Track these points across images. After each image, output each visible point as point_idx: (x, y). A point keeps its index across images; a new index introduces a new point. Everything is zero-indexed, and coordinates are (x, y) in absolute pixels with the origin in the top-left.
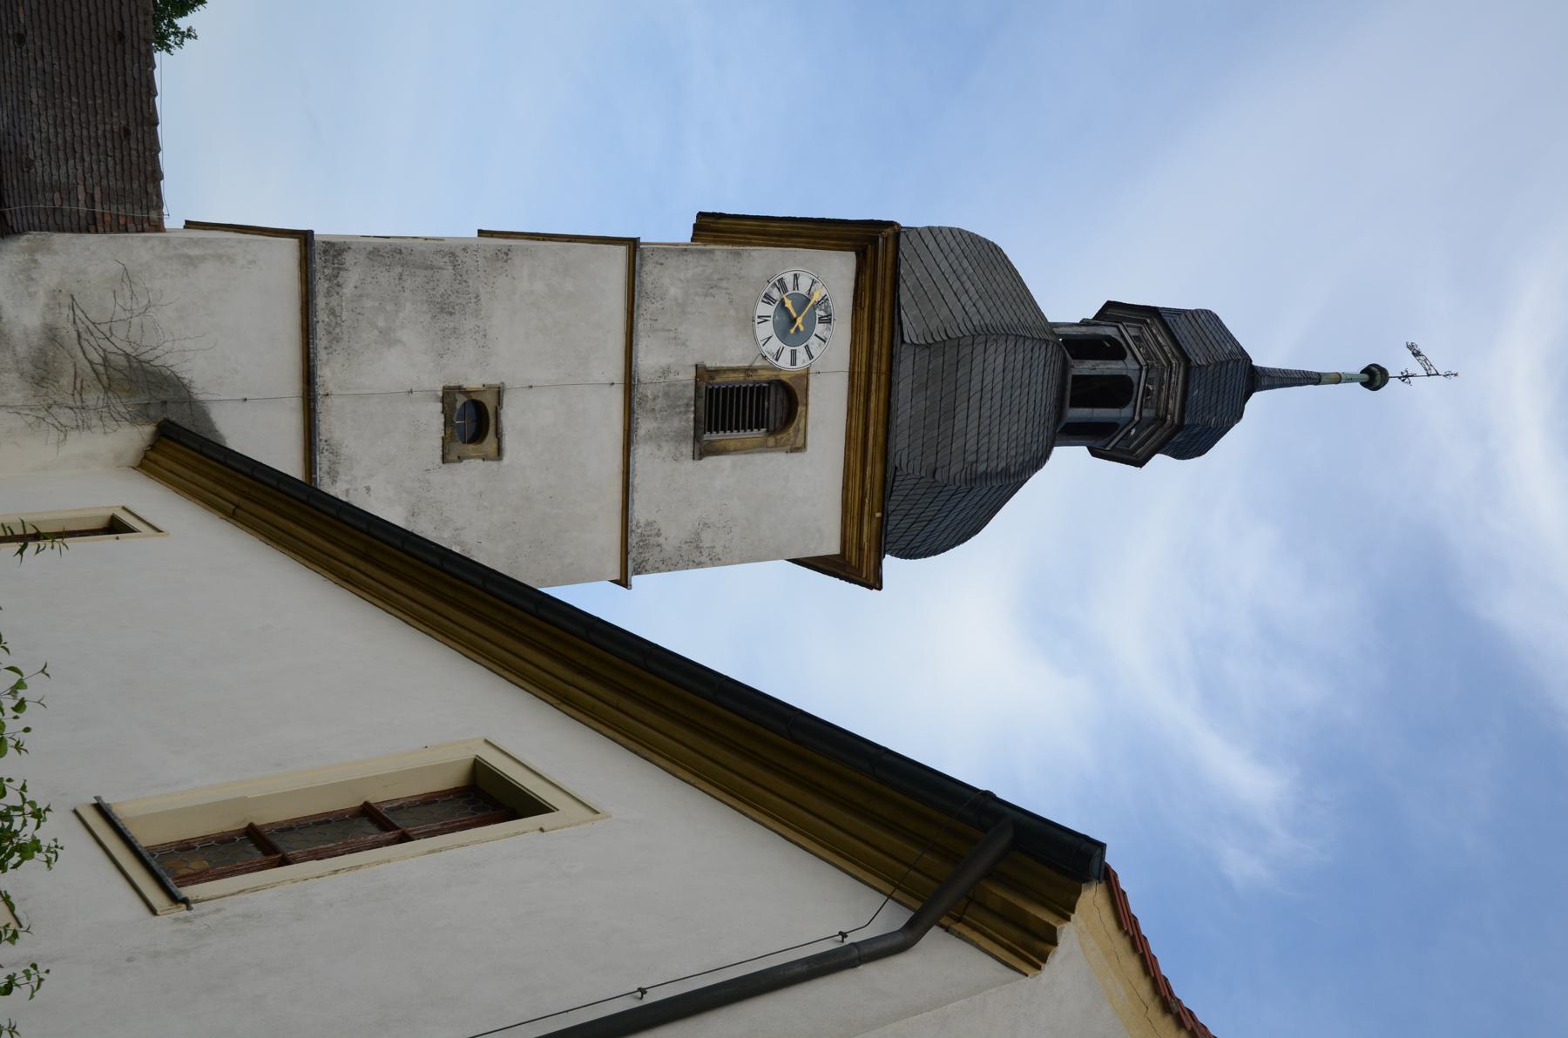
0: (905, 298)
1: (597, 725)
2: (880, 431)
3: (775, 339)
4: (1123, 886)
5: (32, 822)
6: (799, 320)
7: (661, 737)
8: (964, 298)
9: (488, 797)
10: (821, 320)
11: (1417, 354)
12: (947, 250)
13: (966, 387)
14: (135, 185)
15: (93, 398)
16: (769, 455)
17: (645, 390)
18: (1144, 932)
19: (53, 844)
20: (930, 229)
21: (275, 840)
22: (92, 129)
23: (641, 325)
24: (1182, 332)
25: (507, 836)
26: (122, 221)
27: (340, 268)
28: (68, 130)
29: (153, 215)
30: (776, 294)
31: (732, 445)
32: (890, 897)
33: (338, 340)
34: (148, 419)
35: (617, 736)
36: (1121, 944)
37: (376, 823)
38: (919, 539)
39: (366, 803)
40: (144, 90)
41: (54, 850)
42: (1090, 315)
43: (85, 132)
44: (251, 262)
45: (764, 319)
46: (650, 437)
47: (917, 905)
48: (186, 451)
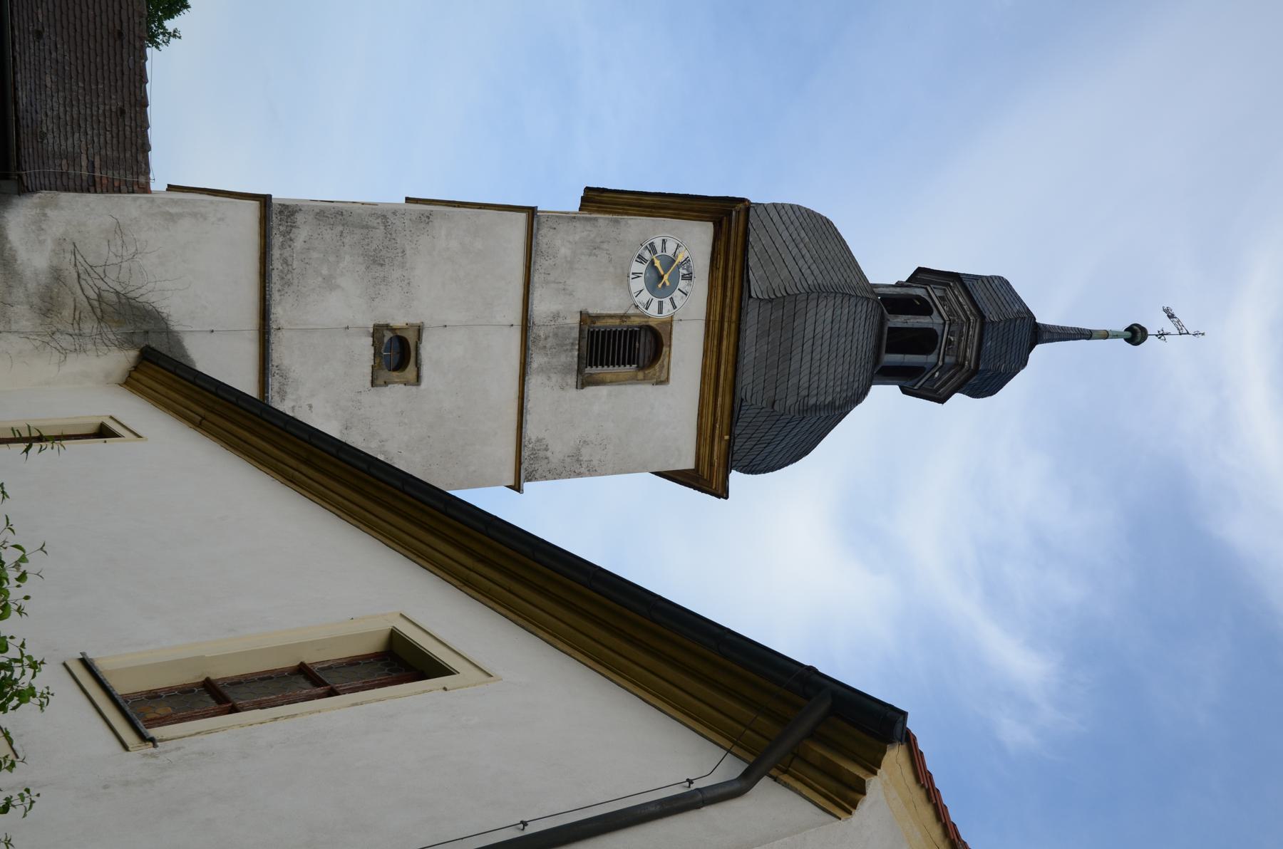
1: (420, 560)
2: (730, 369)
3: (645, 291)
4: (921, 747)
5: (29, 672)
6: (666, 277)
8: (801, 262)
9: (401, 661)
10: (684, 277)
11: (1171, 316)
13: (802, 337)
14: (128, 155)
15: (89, 326)
17: (538, 331)
20: (775, 205)
22: (95, 108)
23: (537, 278)
24: (979, 294)
26: (116, 184)
28: (75, 109)
29: (142, 179)
30: (647, 255)
31: (608, 377)
32: (729, 751)
33: (289, 284)
34: (133, 345)
36: (918, 795)
37: (310, 680)
39: (302, 664)
41: (46, 696)
42: (904, 279)
44: (220, 219)
45: (637, 275)
46: (542, 370)
47: (752, 759)
48: (164, 373)
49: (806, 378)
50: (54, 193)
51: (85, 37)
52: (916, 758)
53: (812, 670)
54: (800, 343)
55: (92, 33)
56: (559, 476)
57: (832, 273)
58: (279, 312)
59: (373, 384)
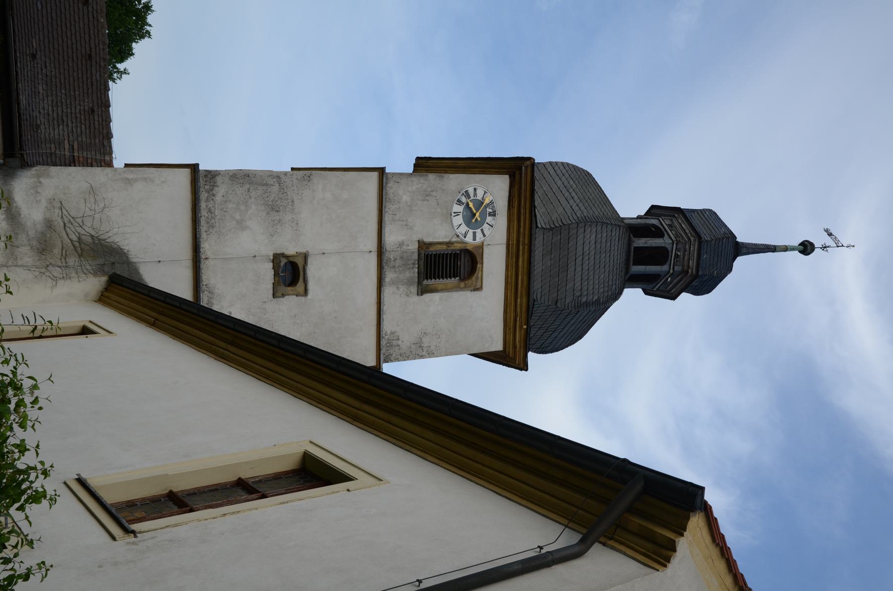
0: (537, 202)
2: (525, 278)
3: (464, 225)
4: (715, 515)
5: (41, 477)
6: (477, 214)
7: (417, 438)
8: (571, 202)
9: (313, 473)
10: (490, 214)
11: (830, 235)
12: (560, 175)
13: (575, 254)
14: (97, 141)
15: (73, 261)
16: (461, 293)
17: (389, 255)
18: (728, 545)
19: (53, 493)
20: (551, 163)
21: (185, 500)
22: (73, 109)
23: (387, 218)
24: (696, 222)
25: (327, 494)
26: (89, 161)
27: (214, 186)
28: (60, 109)
29: (107, 158)
30: (464, 200)
31: (440, 287)
32: (566, 526)
33: (213, 227)
34: (104, 273)
35: (388, 438)
36: (714, 552)
37: (246, 489)
38: (548, 342)
39: (240, 479)
40: (103, 87)
41: (53, 501)
42: (643, 214)
43: (69, 111)
44: (163, 182)
45: (457, 214)
46: (393, 283)
47: (584, 531)
48: (127, 292)
49: (579, 283)
50: (45, 167)
51: (66, 59)
54: (573, 258)
55: (70, 56)
56: (407, 358)
57: (594, 209)
58: (207, 247)
59: (274, 296)
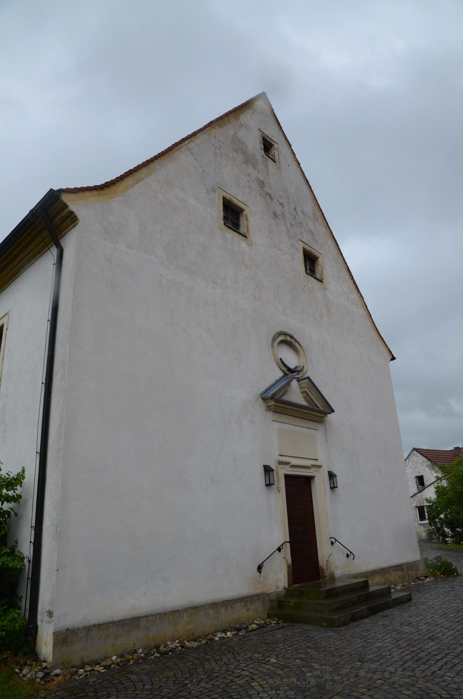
1: (16, 276)
36: (80, 194)
52: (68, 191)
53: (31, 211)
